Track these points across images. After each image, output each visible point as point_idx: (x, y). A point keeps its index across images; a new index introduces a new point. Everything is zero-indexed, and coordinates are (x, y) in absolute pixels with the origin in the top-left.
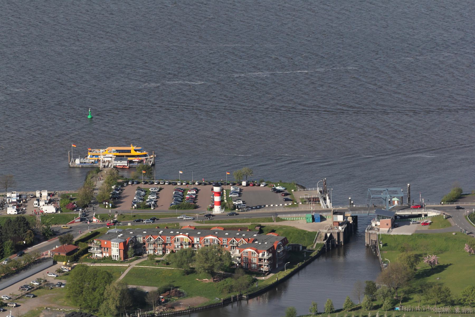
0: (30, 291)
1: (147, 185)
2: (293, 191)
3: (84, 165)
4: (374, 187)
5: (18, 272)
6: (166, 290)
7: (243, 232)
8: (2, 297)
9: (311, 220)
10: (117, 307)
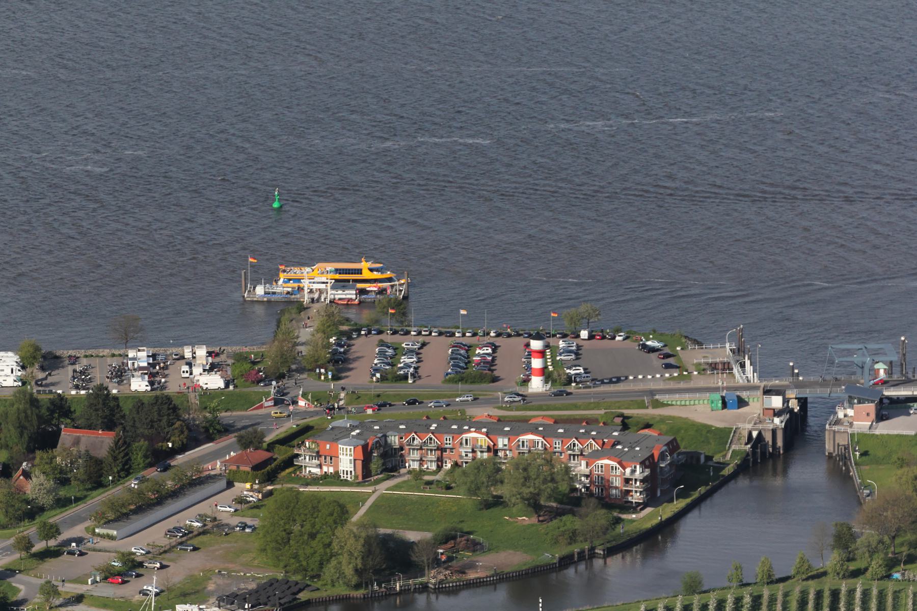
0: (187, 539)
1: (397, 336)
3: (273, 298)
5: (160, 501)
6: (447, 538)
7: (591, 427)
8: (133, 550)
9: (720, 405)
10: (356, 570)
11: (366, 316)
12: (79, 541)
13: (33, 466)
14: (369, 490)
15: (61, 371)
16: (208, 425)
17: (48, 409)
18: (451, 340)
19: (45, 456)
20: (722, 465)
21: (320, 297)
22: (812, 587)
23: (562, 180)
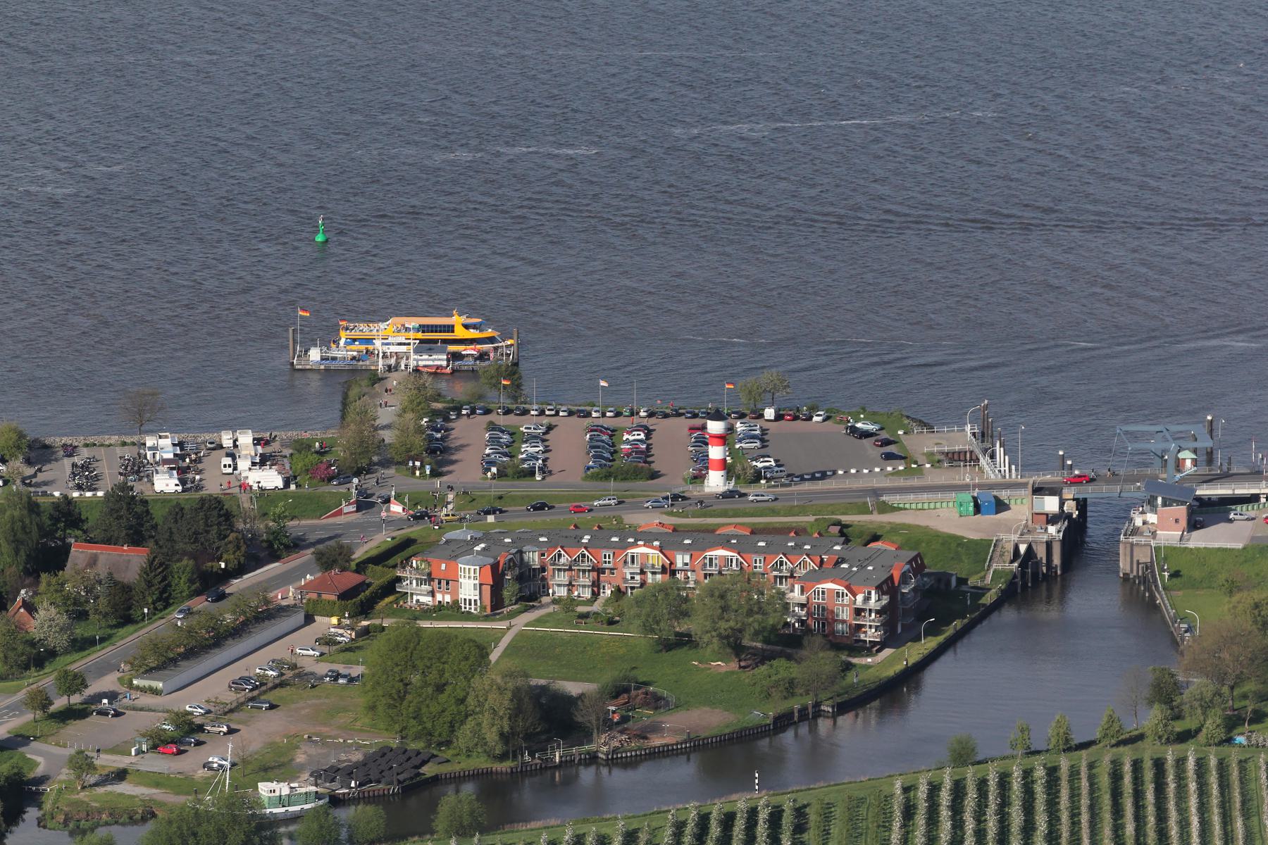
0: (259, 694)
1: (511, 416)
2: (900, 432)
4: (1136, 422)
6: (618, 691)
7: (803, 538)
8: (188, 708)
9: (971, 509)
10: (502, 735)
11: (460, 390)
12: (112, 696)
13: (36, 594)
14: (502, 625)
15: (53, 465)
16: (271, 538)
17: (51, 517)
18: (587, 421)
19: (54, 580)
20: (981, 591)
21: (398, 364)
22: (1127, 756)
23: (1179, 162)
